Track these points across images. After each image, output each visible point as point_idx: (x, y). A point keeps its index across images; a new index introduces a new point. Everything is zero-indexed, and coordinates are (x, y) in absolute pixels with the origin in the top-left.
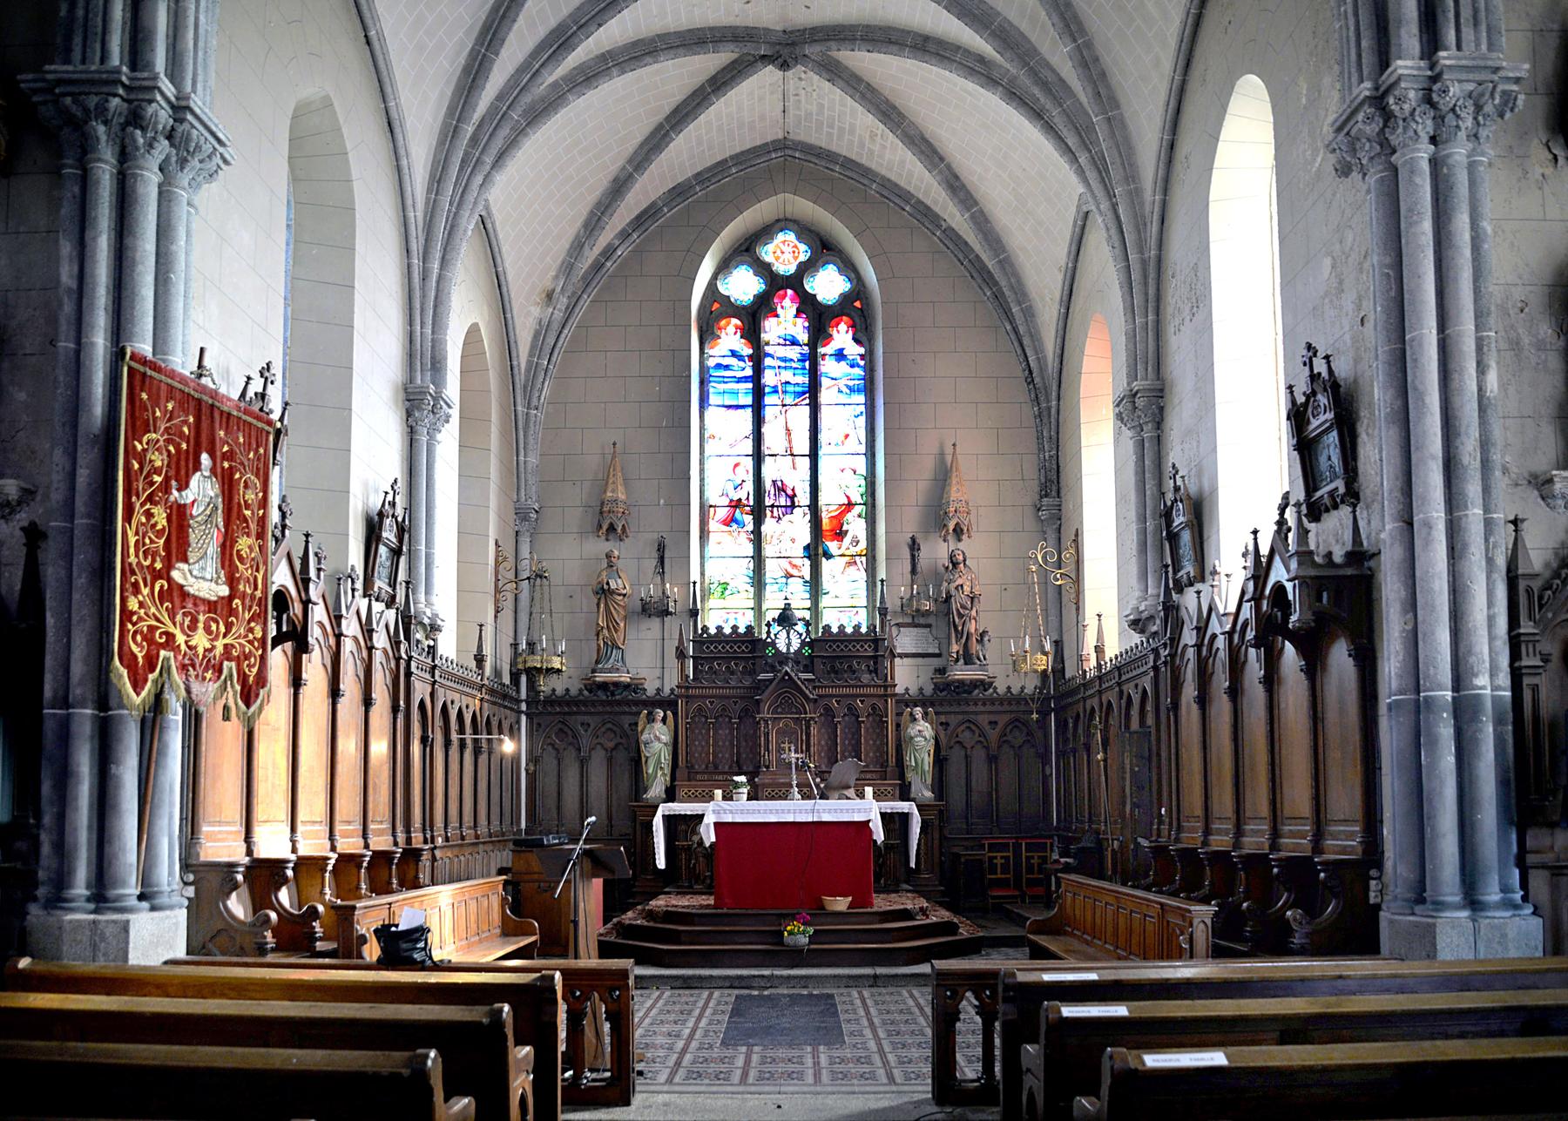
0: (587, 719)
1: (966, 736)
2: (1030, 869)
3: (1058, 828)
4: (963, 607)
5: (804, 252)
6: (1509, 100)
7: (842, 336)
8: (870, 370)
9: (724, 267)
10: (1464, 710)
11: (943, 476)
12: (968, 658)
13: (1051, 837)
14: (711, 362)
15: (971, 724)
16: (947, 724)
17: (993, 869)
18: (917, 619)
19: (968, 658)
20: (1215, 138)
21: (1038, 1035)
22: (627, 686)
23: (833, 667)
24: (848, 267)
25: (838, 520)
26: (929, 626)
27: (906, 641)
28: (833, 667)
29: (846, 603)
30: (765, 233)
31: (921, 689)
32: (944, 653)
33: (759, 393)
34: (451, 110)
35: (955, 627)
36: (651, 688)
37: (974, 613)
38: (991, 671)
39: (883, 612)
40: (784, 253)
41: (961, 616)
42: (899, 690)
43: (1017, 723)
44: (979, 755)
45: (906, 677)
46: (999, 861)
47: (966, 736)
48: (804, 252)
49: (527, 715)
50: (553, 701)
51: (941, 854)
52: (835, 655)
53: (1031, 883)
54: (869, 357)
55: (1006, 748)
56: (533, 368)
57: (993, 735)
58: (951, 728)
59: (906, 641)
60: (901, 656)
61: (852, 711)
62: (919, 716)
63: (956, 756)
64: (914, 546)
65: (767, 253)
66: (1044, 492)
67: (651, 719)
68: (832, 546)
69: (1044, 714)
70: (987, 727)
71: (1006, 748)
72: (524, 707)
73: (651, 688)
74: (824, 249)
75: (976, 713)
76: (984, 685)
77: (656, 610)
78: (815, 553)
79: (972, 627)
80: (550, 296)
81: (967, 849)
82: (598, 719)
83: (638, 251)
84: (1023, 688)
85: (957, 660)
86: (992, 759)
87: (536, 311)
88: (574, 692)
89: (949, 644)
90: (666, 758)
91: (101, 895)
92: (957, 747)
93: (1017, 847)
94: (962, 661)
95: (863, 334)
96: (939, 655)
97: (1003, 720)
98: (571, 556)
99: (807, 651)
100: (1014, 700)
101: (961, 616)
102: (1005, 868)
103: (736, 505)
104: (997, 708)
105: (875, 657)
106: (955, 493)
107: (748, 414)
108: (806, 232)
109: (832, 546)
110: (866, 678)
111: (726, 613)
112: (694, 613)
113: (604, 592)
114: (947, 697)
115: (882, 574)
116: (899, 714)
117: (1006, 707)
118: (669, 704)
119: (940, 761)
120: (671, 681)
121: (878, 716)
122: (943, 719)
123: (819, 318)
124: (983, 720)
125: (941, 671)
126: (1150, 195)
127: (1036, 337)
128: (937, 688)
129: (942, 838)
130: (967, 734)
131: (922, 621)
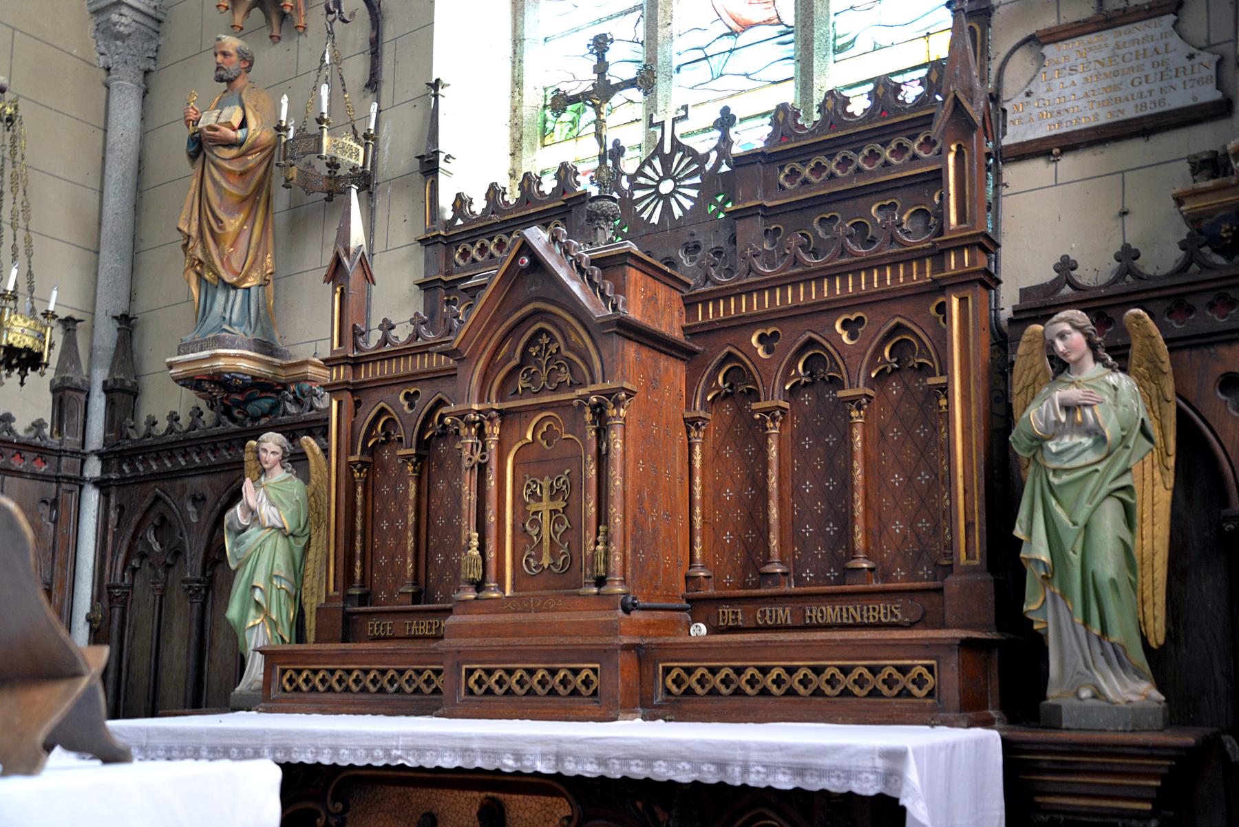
0: (198, 483)
22: (260, 386)
31: (1127, 255)
45: (1046, 225)
49: (102, 485)
61: (820, 369)
72: (94, 468)
128: (1201, 234)
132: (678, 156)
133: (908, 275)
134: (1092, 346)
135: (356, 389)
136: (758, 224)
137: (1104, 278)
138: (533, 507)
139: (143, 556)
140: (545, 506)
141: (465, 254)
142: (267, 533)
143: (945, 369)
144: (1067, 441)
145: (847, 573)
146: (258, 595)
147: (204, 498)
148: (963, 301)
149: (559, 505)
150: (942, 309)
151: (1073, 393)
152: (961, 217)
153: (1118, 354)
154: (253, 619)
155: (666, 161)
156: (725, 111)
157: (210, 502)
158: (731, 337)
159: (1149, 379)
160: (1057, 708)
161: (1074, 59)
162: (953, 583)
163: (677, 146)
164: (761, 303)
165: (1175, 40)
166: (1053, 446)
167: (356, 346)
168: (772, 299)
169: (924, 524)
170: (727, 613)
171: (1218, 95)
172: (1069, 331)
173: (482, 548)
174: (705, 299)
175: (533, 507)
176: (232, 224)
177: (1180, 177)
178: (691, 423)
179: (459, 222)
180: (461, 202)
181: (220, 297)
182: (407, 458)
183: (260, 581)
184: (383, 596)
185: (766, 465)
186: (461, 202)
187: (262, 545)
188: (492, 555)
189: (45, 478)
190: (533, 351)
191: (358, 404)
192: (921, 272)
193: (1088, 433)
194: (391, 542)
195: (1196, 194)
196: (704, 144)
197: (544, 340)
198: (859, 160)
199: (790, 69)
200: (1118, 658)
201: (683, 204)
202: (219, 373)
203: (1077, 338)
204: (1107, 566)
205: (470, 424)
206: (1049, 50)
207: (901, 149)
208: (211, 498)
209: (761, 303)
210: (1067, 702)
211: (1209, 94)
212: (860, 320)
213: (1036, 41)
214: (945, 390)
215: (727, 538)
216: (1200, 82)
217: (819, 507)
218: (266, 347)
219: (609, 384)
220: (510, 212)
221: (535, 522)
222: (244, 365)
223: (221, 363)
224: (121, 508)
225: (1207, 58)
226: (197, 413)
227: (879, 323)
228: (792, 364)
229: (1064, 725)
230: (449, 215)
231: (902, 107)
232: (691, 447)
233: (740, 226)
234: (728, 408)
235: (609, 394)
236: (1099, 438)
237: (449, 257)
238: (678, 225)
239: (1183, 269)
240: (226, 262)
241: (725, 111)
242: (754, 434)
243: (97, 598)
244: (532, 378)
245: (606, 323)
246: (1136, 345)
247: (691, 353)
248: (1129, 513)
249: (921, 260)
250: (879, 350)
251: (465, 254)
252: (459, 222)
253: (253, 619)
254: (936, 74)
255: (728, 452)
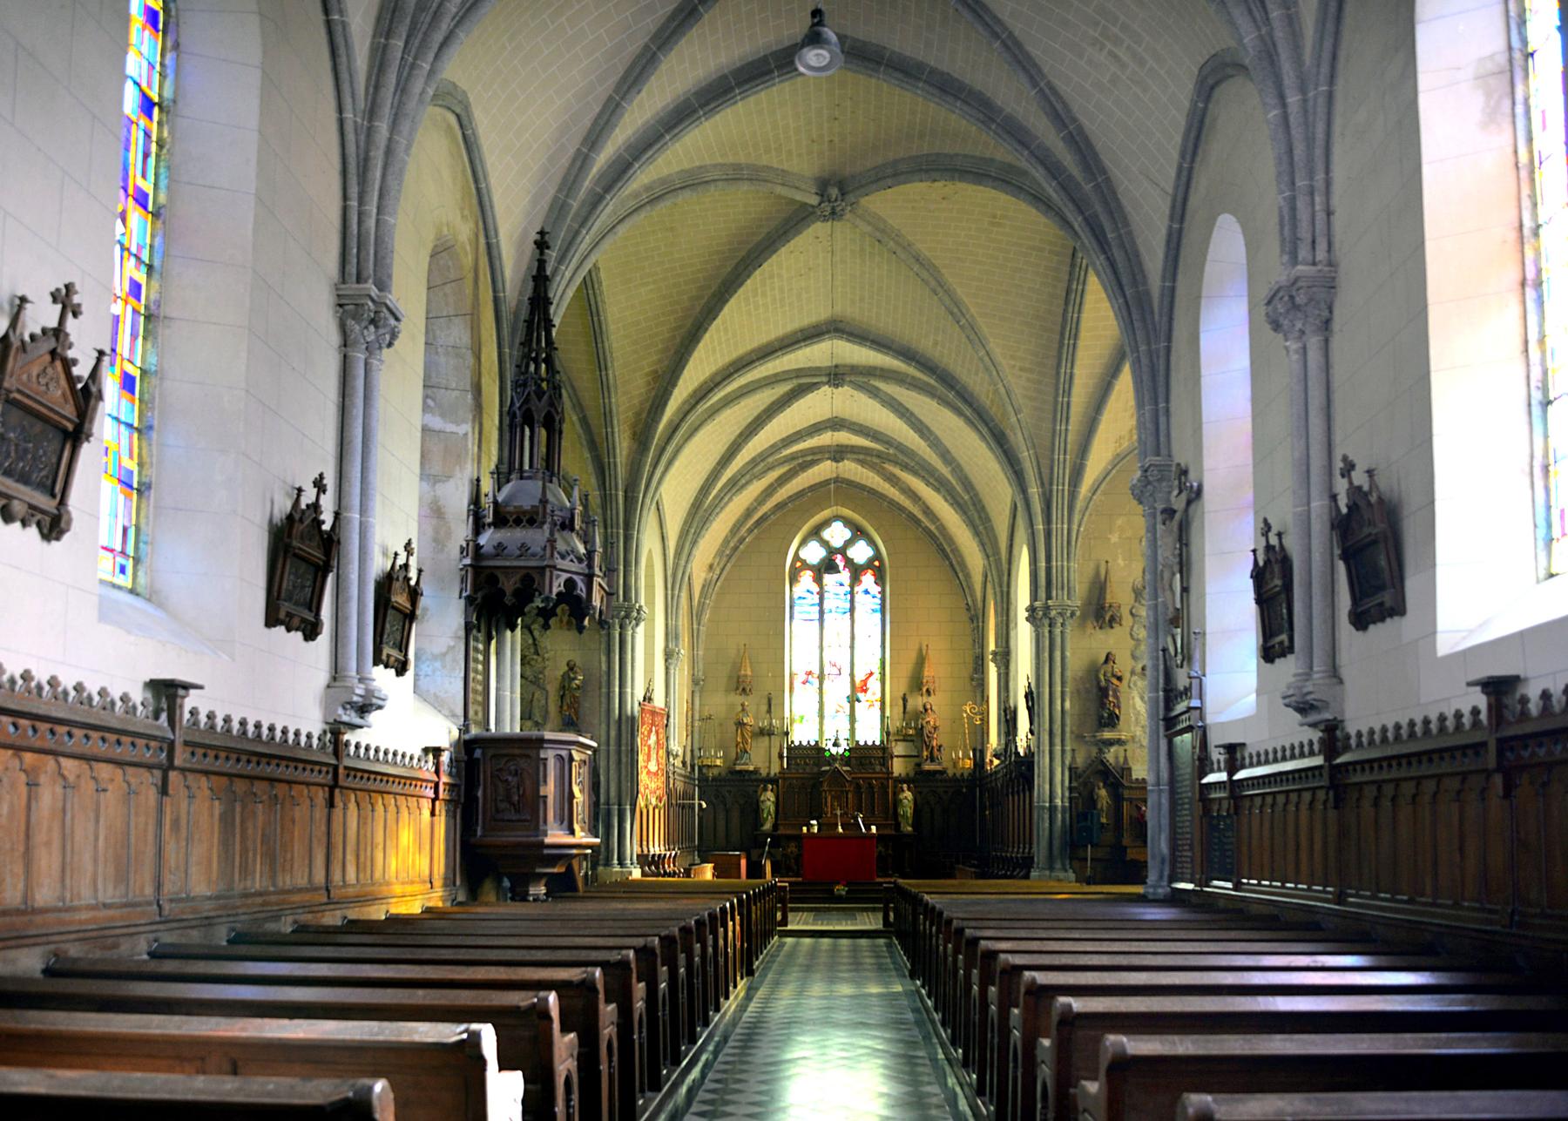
5: (847, 534)
6: (1073, 614)
7: (868, 579)
8: (883, 599)
9: (803, 542)
10: (1052, 809)
11: (921, 661)
12: (932, 759)
14: (795, 596)
18: (906, 739)
19: (932, 759)
20: (1200, 279)
21: (1096, 1070)
24: (872, 543)
25: (865, 682)
29: (870, 732)
30: (826, 523)
33: (822, 613)
34: (685, 523)
36: (764, 772)
38: (945, 765)
39: (888, 734)
40: (837, 534)
42: (896, 774)
45: (898, 767)
48: (847, 534)
52: (861, 755)
54: (883, 592)
56: (702, 605)
59: (899, 749)
61: (871, 786)
64: (905, 700)
65: (827, 534)
66: (976, 671)
67: (765, 789)
68: (861, 695)
73: (764, 772)
74: (858, 532)
76: (943, 772)
77: (766, 732)
78: (853, 700)
80: (711, 567)
83: (757, 538)
87: (703, 575)
90: (772, 809)
91: (621, 863)
95: (880, 579)
98: (720, 702)
100: (954, 779)
103: (809, 673)
106: (928, 673)
107: (817, 623)
108: (848, 523)
109: (861, 695)
110: (878, 768)
111: (803, 734)
112: (787, 734)
113: (740, 724)
115: (888, 713)
118: (774, 781)
120: (775, 769)
121: (884, 788)
123: (856, 572)
125: (918, 765)
126: (1005, 566)
127: (971, 588)
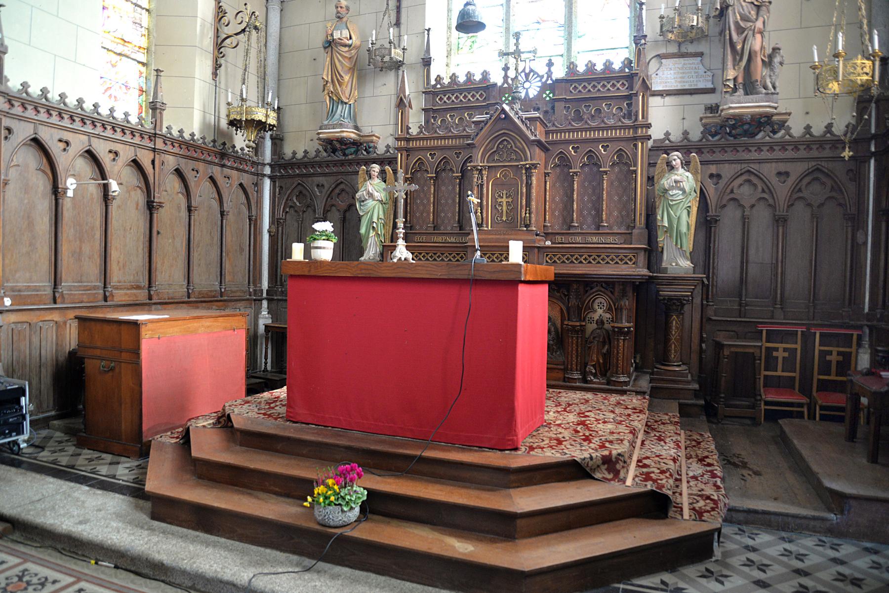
0: (321, 180)
1: (745, 193)
2: (825, 368)
3: (869, 317)
4: (745, 19)
13: (860, 327)
15: (750, 176)
16: (719, 176)
17: (771, 362)
19: (749, 86)
22: (356, 144)
23: (577, 112)
26: (701, 54)
27: (665, 75)
28: (577, 112)
31: (686, 133)
32: (719, 87)
35: (733, 45)
37: (759, 24)
41: (740, 30)
43: (815, 174)
44: (761, 218)
45: (663, 119)
46: (780, 355)
47: (745, 193)
49: (272, 178)
50: (293, 164)
51: (702, 340)
53: (824, 386)
55: (799, 206)
57: (782, 190)
58: (722, 183)
59: (665, 75)
60: (661, 94)
61: (593, 161)
62: (677, 162)
63: (729, 220)
69: (860, 160)
70: (774, 180)
71: (799, 206)
72: (268, 170)
75: (760, 161)
76: (764, 122)
79: (756, 43)
81: (738, 337)
82: (331, 179)
84: (829, 127)
85: (735, 90)
86: (780, 221)
88: (312, 154)
89: (724, 69)
92: (731, 207)
93: (807, 338)
94: (741, 92)
96: (712, 91)
97: (797, 170)
99: (548, 96)
101: (740, 30)
102: (789, 363)
104: (789, 154)
105: (629, 97)
114: (727, 138)
116: (652, 165)
117: (802, 153)
119: (707, 222)
122: (713, 169)
124: (769, 171)
128: (708, 131)
129: (705, 320)
130: (746, 189)
131: (691, 49)
132: (532, 74)
133: (624, 133)
134: (682, 163)
135: (408, 150)
136: (562, 104)
137: (679, 139)
138: (499, 200)
139: (291, 207)
140: (504, 200)
141: (441, 99)
142: (375, 203)
143: (635, 165)
144: (675, 192)
145: (570, 227)
146: (375, 225)
147: (323, 185)
148: (642, 143)
149: (510, 200)
150: (636, 146)
151: (678, 178)
152: (643, 117)
153: (686, 164)
154: (372, 233)
155: (527, 75)
156: (550, 60)
157: (326, 188)
158: (563, 146)
159: (695, 174)
160: (666, 268)
161: (671, 66)
162: (635, 231)
163: (531, 71)
164: (573, 136)
165: (701, 66)
166: (670, 192)
167: (408, 133)
168: (577, 135)
169: (624, 213)
170: (559, 238)
171: (712, 86)
172: (676, 157)
173: (481, 213)
174: (553, 132)
175: (499, 200)
176: (347, 78)
177: (700, 112)
178: (546, 174)
179: (439, 86)
180: (439, 79)
181: (340, 107)
182: (432, 177)
183: (375, 220)
184: (418, 227)
185: (573, 190)
186: (439, 79)
187: (374, 207)
188: (485, 215)
189: (252, 173)
190: (501, 146)
191: (408, 155)
192: (629, 133)
193: (680, 190)
194: (421, 208)
195: (706, 117)
196: (542, 70)
197: (505, 143)
198: (599, 87)
199: (562, 40)
200: (683, 254)
201: (533, 93)
202: (343, 138)
203: (679, 161)
204: (684, 229)
205: (477, 170)
206: (664, 61)
207: (614, 85)
208: (327, 186)
209: (573, 136)
210: (669, 266)
211: (709, 85)
212: (608, 146)
213: (660, 57)
214: (635, 172)
215: (557, 213)
216: (707, 81)
217: (590, 205)
218: (356, 128)
219: (534, 162)
220: (461, 85)
221: (500, 205)
222: (353, 135)
223: (344, 134)
224: (281, 187)
225: (709, 73)
226: (318, 151)
227: (614, 147)
228: (583, 158)
229: (545, 288)
230: (433, 82)
231: (614, 71)
232: (546, 182)
233: (556, 104)
234: (558, 170)
235: (533, 165)
236: (684, 192)
237: (434, 99)
238: (531, 100)
239: (701, 140)
240: (344, 93)
241: (550, 60)
242: (569, 180)
243: (272, 223)
244: (501, 156)
245: (534, 141)
246: (692, 164)
247: (548, 150)
248: (689, 213)
249: (629, 129)
250: (613, 156)
251: (441, 99)
252: (439, 86)
253: (372, 233)
254: (628, 63)
255: (558, 185)
